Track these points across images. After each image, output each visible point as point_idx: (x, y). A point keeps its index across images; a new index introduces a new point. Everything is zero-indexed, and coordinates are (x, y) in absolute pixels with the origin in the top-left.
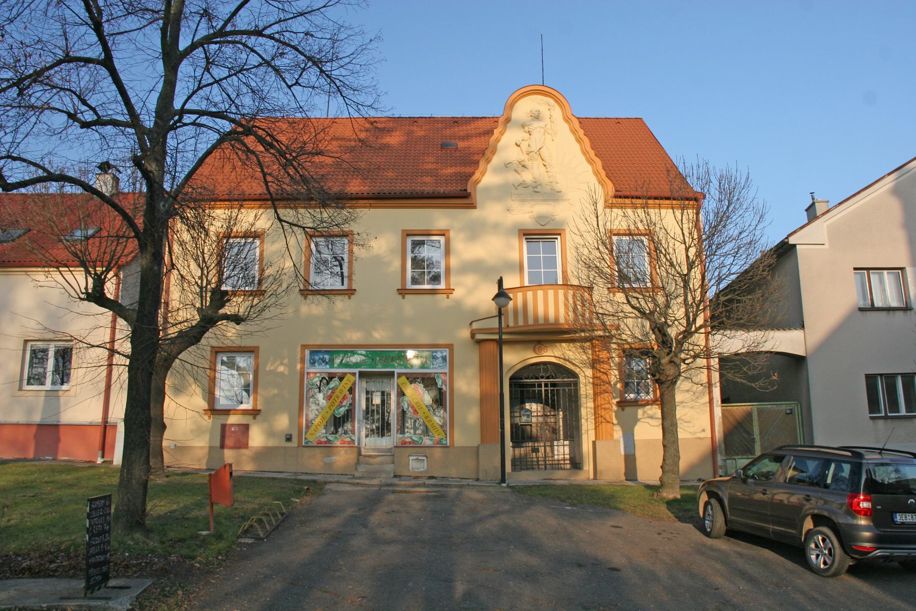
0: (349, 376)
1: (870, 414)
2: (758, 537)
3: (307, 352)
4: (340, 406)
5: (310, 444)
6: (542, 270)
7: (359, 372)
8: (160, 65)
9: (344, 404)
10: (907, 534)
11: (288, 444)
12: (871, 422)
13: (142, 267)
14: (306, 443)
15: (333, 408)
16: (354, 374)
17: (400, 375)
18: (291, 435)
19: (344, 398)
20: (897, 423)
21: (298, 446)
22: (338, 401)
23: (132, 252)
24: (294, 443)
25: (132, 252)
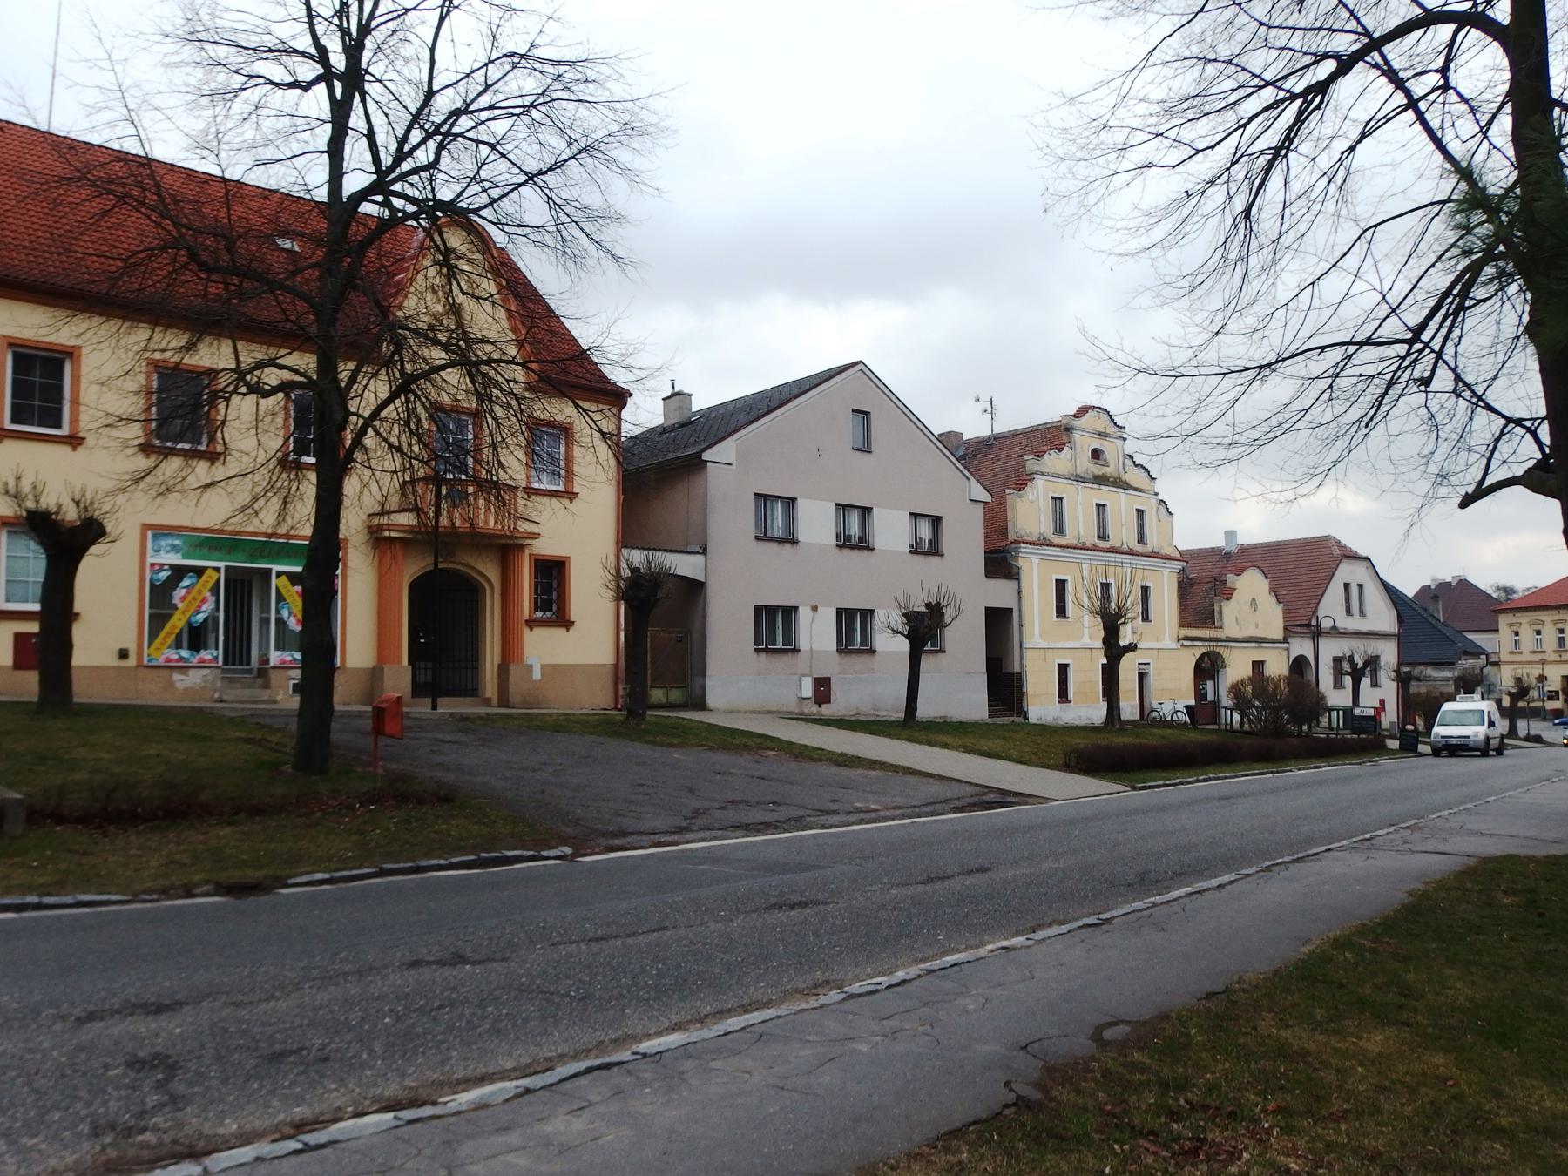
0: (209, 572)
1: (543, 667)
2: (724, 747)
3: (150, 534)
4: (198, 612)
5: (154, 663)
6: (37, 403)
7: (227, 567)
8: (1453, 383)
9: (203, 609)
10: (69, 900)
11: (124, 663)
12: (755, 654)
13: (1467, 493)
14: (149, 661)
15: (188, 614)
16: (217, 569)
17: (279, 574)
18: (127, 650)
19: (204, 601)
20: (777, 657)
21: (138, 666)
22: (196, 604)
23: (296, 372)
24: (131, 662)
25: (296, 372)
